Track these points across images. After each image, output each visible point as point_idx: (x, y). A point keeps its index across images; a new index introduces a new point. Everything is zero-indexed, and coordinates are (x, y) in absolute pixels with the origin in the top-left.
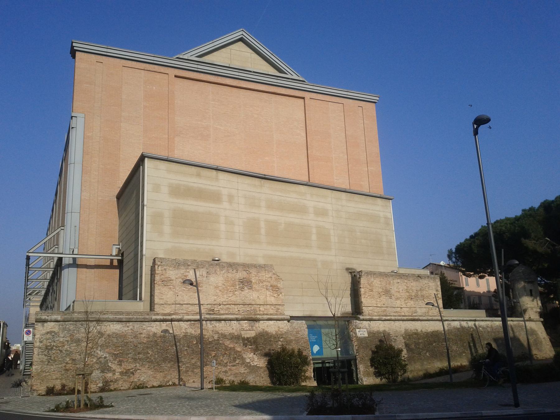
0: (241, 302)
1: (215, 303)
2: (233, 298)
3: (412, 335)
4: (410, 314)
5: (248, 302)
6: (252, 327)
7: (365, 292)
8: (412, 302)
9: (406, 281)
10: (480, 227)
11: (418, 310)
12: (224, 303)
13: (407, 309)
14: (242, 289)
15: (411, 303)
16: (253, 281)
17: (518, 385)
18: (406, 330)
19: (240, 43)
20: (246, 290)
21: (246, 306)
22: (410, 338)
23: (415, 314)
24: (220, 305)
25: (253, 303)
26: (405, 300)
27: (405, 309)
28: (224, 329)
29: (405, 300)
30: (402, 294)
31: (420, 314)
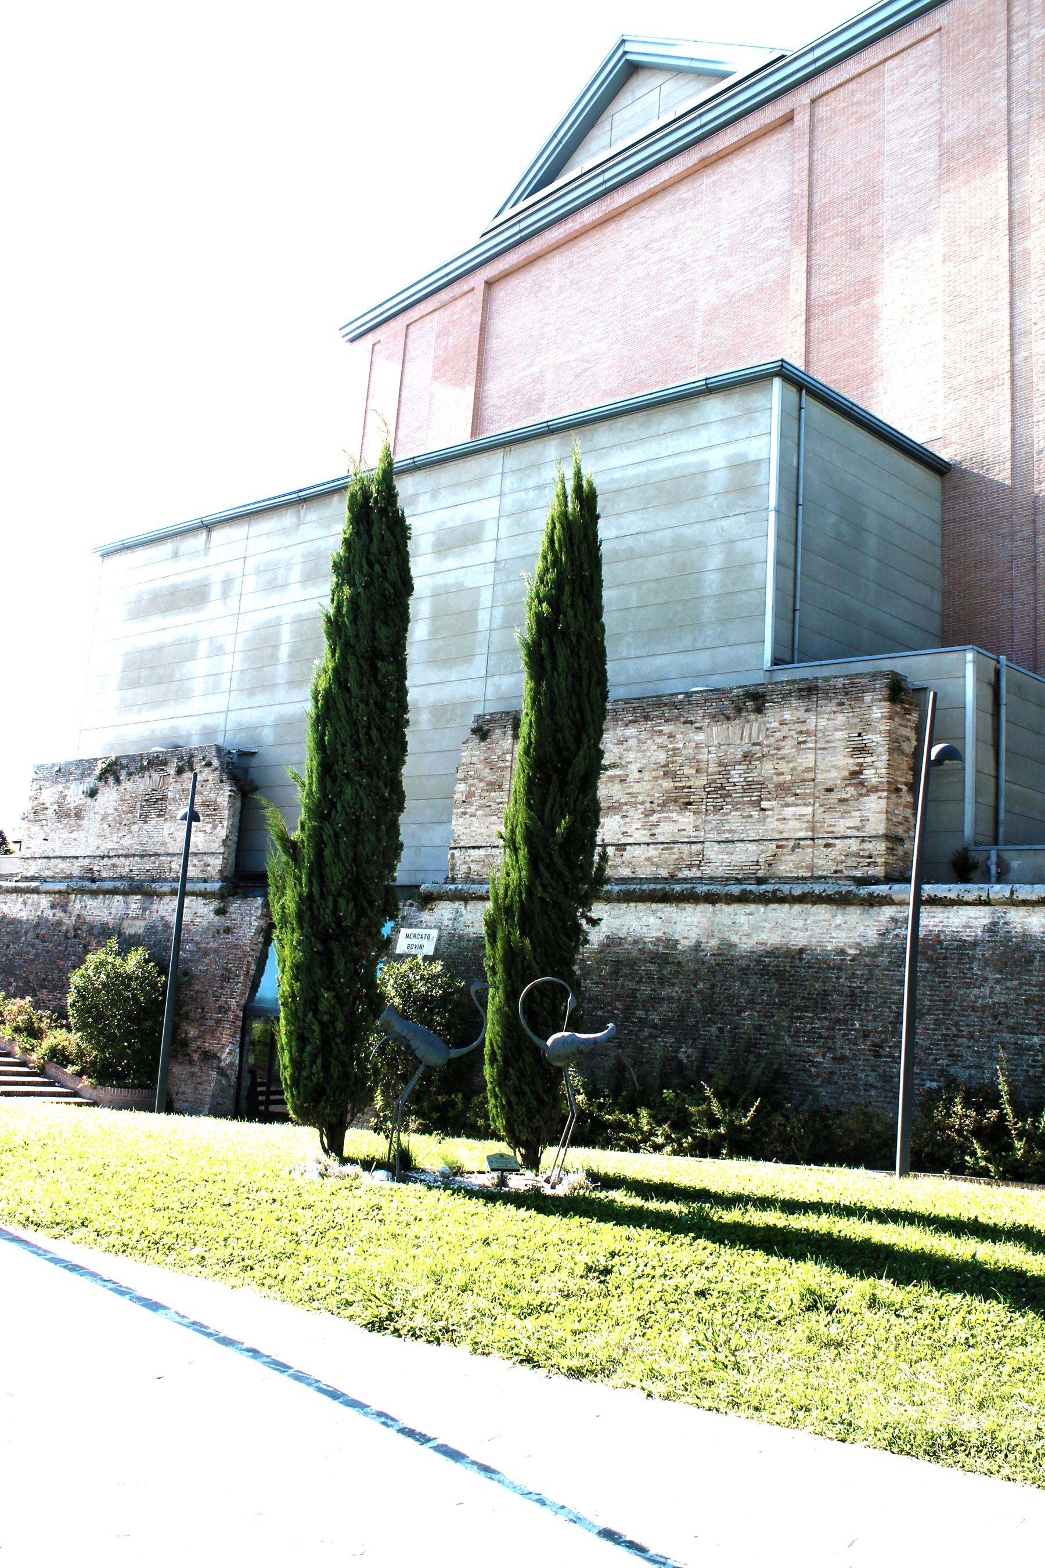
0: (139, 849)
1: (99, 853)
2: (127, 842)
3: (633, 963)
4: (664, 873)
5: (151, 849)
6: (145, 910)
7: (470, 794)
8: (686, 821)
9: (667, 728)
10: (945, 1215)
11: (713, 852)
12: (111, 854)
13: (652, 852)
14: (145, 818)
15: (682, 823)
16: (170, 795)
17: (402, 875)
18: (204, 727)
19: (411, 328)
20: (154, 820)
21: (146, 859)
22: (615, 973)
23: (694, 873)
24: (102, 857)
25: (162, 851)
26: (648, 814)
27: (637, 851)
28: (96, 912)
29: (648, 814)
30: (636, 788)
31: (720, 873)
